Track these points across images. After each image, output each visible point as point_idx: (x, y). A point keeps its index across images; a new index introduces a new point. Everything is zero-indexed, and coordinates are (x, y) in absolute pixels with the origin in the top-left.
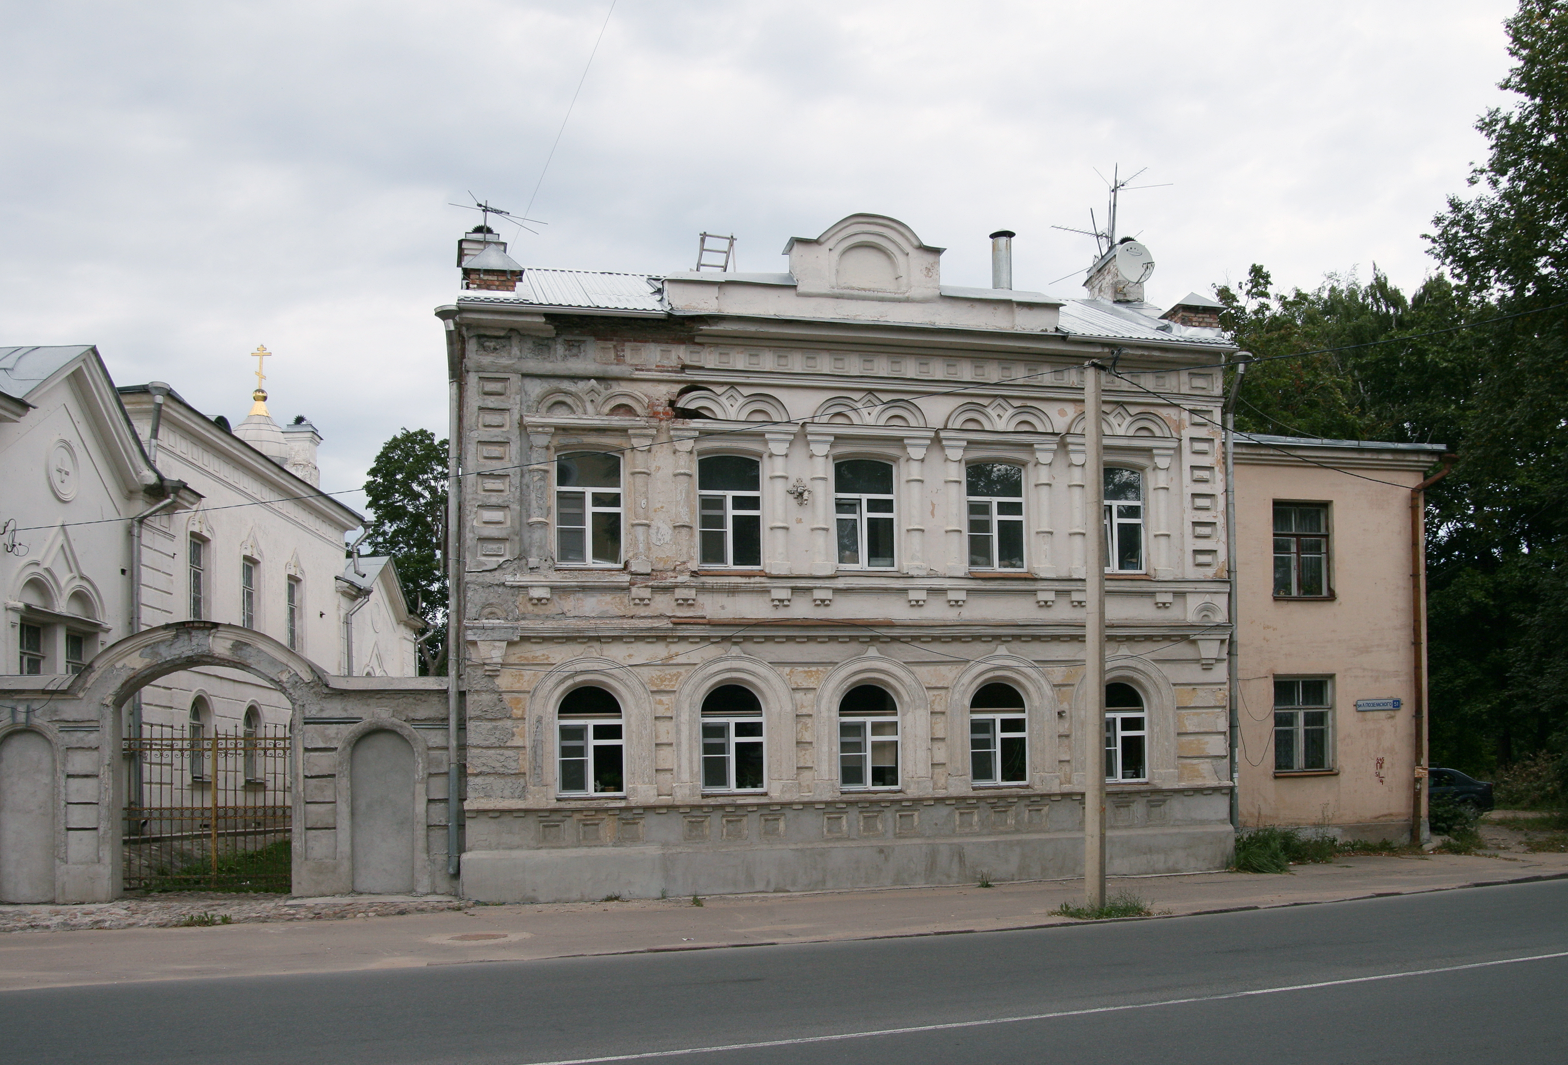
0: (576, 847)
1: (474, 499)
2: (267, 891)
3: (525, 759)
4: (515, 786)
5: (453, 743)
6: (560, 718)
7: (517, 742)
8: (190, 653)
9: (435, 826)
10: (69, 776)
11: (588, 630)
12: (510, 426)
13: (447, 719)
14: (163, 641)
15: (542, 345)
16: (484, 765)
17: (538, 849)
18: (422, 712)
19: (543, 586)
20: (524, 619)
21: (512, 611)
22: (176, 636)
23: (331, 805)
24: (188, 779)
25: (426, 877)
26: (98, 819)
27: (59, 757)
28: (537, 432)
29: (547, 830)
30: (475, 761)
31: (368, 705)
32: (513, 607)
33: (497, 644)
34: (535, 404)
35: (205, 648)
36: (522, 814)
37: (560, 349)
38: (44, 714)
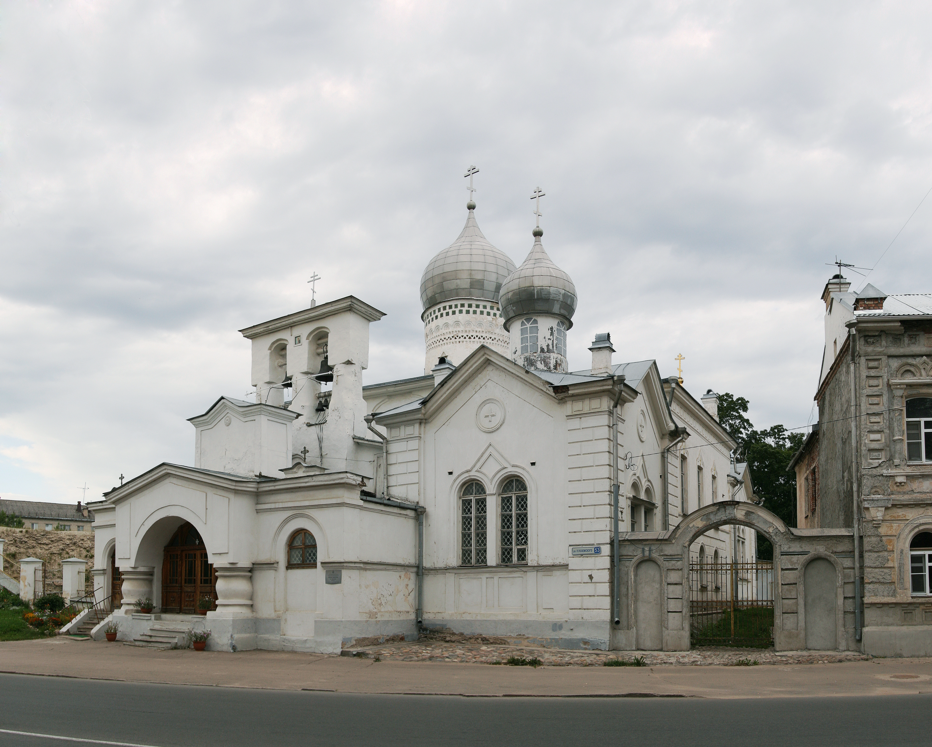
0: (921, 625)
1: (865, 428)
2: (751, 647)
3: (894, 574)
4: (890, 590)
5: (857, 565)
6: (911, 550)
7: (890, 564)
8: (725, 518)
9: (847, 612)
10: (668, 584)
11: (927, 500)
12: (883, 386)
13: (854, 552)
14: (712, 512)
15: (896, 338)
16: (874, 577)
17: (902, 625)
18: (840, 548)
19: (902, 475)
20: (892, 494)
21: (887, 490)
22: (718, 510)
23: (794, 601)
24: (699, 587)
25: (844, 641)
26: (682, 606)
27: (664, 574)
28: (897, 388)
29: (906, 615)
30: (870, 575)
31: (813, 544)
32: (887, 488)
33: (880, 509)
34: (895, 372)
35: (733, 515)
36: (893, 606)
37: (906, 340)
38: (656, 552)
